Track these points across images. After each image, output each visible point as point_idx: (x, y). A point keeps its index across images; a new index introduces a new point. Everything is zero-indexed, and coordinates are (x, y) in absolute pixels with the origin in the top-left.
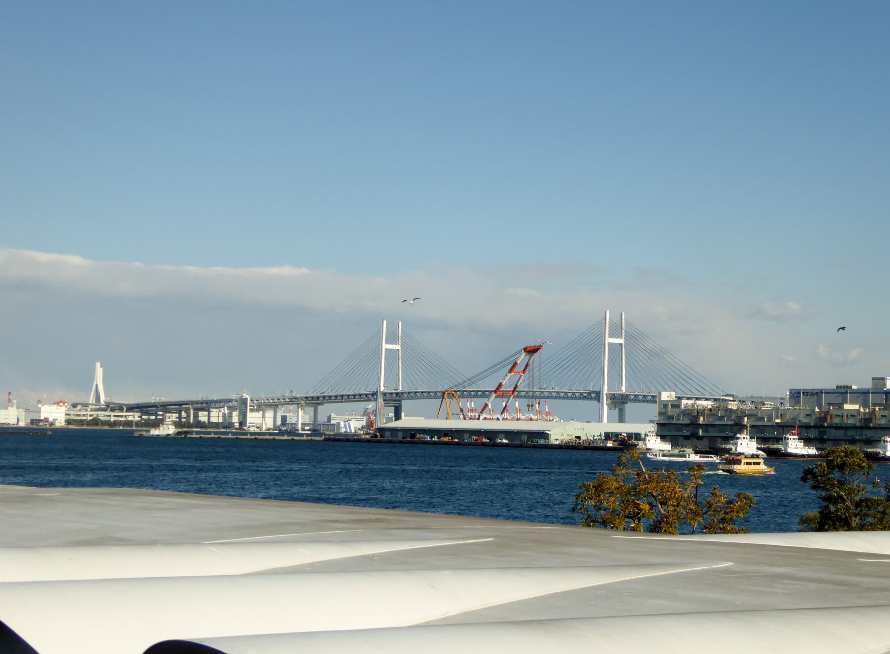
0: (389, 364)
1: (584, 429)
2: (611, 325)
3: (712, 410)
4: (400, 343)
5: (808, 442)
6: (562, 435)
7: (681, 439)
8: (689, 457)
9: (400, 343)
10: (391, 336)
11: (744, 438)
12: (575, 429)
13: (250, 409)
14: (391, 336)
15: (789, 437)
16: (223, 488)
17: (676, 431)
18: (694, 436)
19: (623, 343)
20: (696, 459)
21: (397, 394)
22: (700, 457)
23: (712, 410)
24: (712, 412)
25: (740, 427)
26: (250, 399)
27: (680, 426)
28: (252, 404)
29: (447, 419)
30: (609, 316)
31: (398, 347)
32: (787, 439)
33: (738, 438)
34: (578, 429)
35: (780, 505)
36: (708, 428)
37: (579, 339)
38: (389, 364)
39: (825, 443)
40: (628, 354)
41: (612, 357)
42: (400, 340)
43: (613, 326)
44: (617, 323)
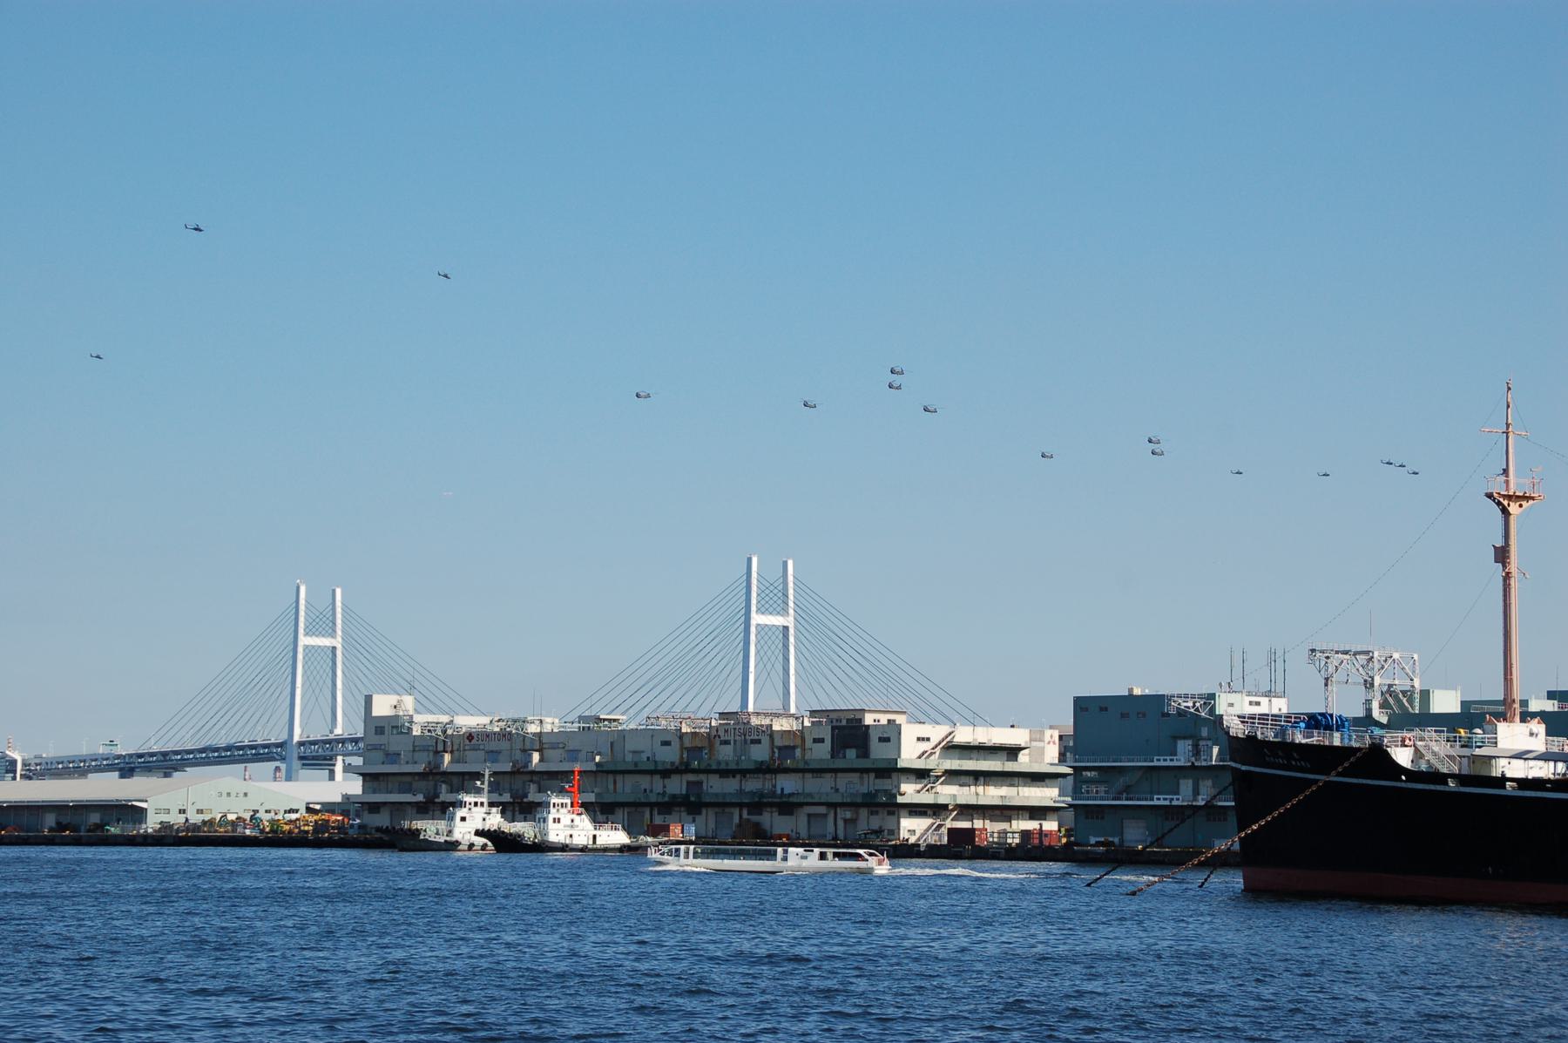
0: (311, 678)
1: (246, 794)
2: (308, 624)
3: (473, 738)
4: (791, 612)
5: (601, 812)
6: (182, 811)
7: (409, 810)
8: (785, 859)
9: (791, 612)
10: (318, 620)
11: (476, 804)
12: (221, 794)
13: (21, 775)
14: (318, 620)
15: (554, 800)
16: (372, 1017)
17: (401, 791)
18: (691, 805)
19: (339, 647)
20: (805, 863)
21: (329, 742)
22: (805, 851)
23: (473, 738)
24: (474, 741)
25: (465, 781)
26: (23, 760)
27: (409, 779)
28: (28, 773)
29: (383, 763)
30: (794, 572)
31: (789, 621)
32: (545, 805)
33: (461, 804)
34: (229, 794)
35: (6, 880)
36: (466, 782)
37: (379, 636)
38: (311, 678)
39: (531, 813)
40: (347, 667)
41: (309, 673)
42: (791, 604)
43: (767, 592)
44: (776, 585)
